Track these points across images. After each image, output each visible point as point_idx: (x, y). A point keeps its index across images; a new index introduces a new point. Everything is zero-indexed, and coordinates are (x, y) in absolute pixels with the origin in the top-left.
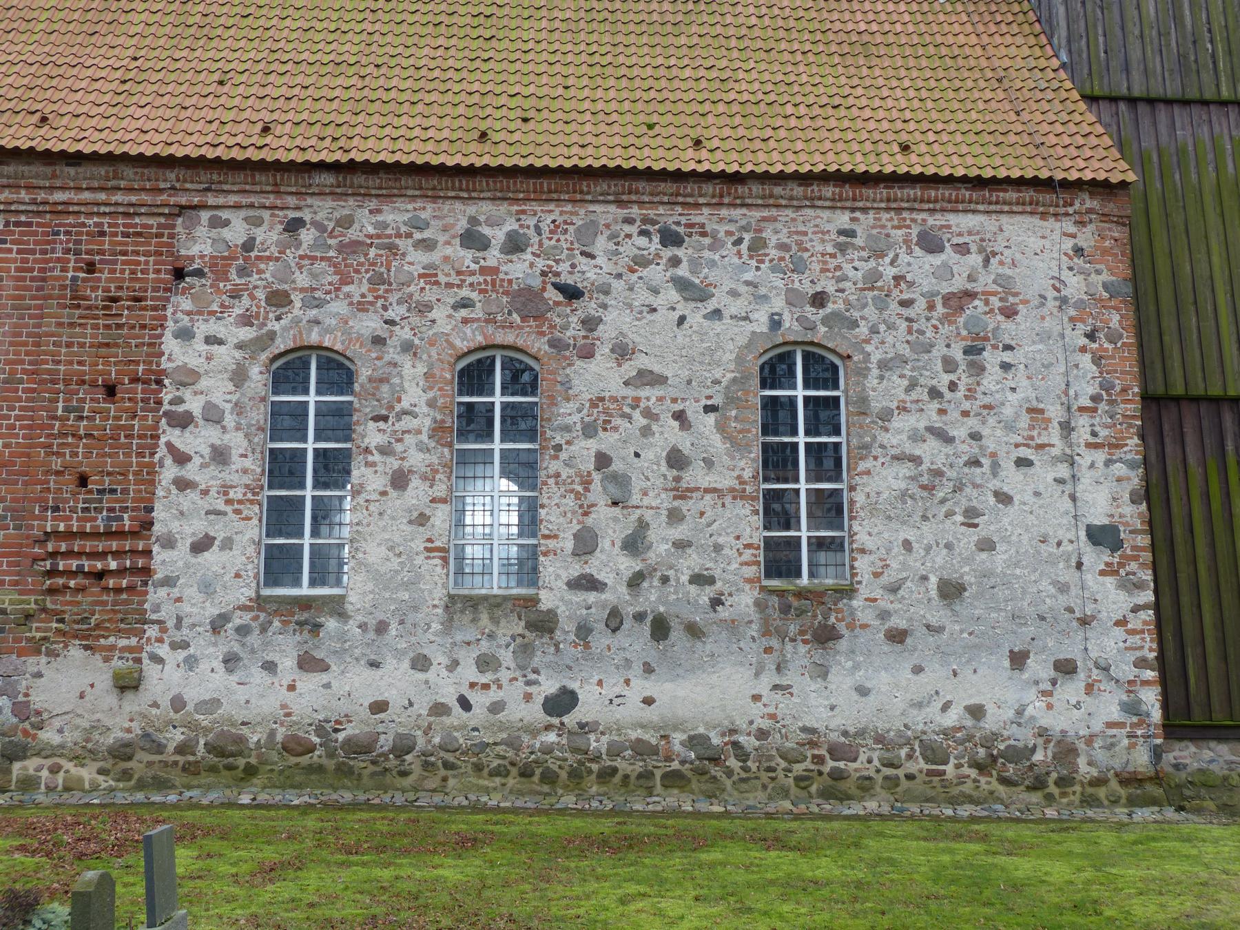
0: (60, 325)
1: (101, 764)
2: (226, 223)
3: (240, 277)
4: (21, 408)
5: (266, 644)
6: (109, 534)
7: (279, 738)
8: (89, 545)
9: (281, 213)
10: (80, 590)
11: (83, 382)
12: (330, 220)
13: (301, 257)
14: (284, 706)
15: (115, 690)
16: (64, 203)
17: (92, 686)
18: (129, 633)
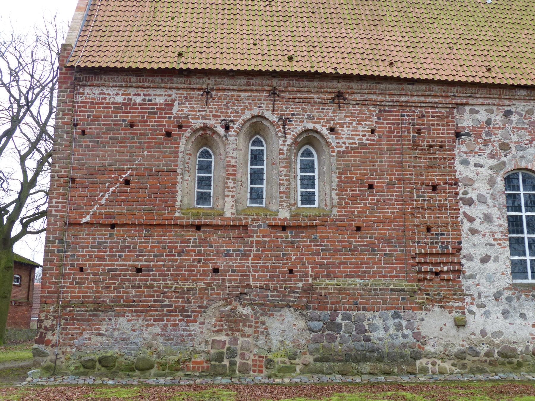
0: (410, 157)
1: (452, 361)
2: (478, 112)
3: (487, 136)
4: (397, 196)
5: (521, 305)
6: (443, 254)
7: (531, 349)
8: (434, 259)
9: (501, 108)
10: (431, 280)
11: (423, 184)
12: (523, 111)
13: (514, 128)
14: (531, 334)
15: (455, 327)
16: (406, 102)
17: (445, 325)
18: (458, 300)
